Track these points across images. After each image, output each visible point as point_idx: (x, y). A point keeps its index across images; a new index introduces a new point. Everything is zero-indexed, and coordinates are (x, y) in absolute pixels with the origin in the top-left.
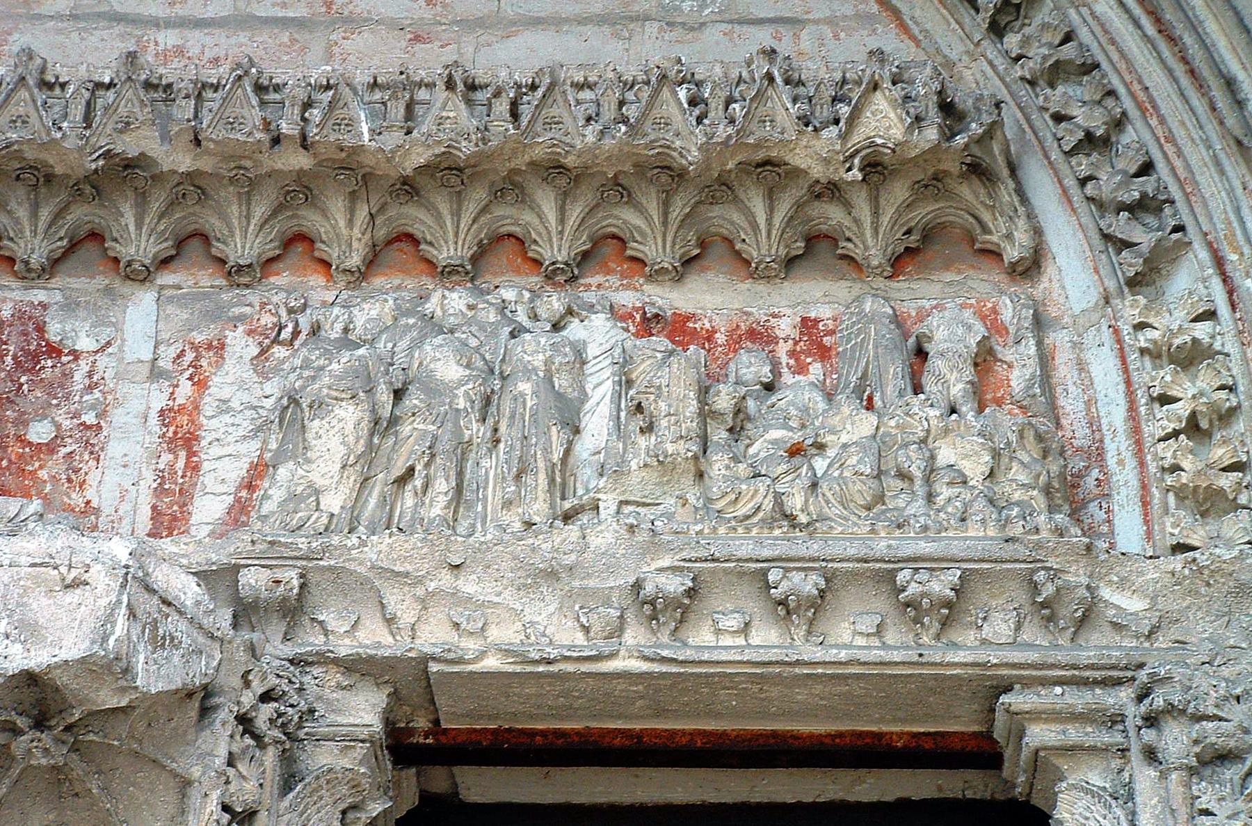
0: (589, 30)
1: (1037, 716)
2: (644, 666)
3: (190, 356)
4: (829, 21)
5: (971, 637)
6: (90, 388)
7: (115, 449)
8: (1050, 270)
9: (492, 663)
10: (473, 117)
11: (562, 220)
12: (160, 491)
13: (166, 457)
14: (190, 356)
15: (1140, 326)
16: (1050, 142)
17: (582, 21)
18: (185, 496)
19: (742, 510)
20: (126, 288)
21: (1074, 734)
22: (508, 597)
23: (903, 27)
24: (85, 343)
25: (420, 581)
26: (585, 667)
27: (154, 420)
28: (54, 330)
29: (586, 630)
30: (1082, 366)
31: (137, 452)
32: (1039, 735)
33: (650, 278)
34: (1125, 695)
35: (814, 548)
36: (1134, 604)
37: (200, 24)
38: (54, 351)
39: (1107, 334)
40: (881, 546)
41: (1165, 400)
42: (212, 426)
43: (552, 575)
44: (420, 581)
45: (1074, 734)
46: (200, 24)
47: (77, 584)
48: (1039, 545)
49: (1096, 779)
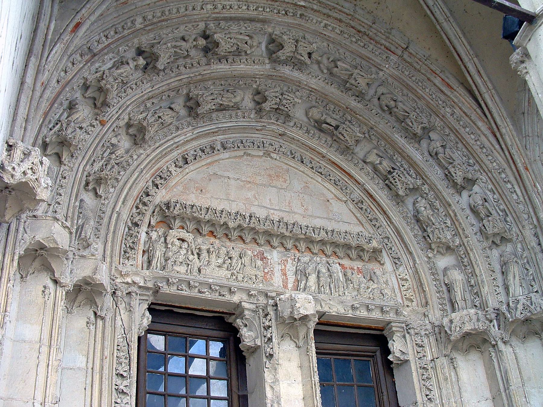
0: (325, 220)
1: (394, 326)
2: (352, 316)
3: (283, 262)
4: (354, 224)
5: (388, 316)
6: (271, 264)
7: (276, 274)
8: (385, 265)
9: (334, 314)
10: (46, 156)
11: (329, 249)
12: (283, 282)
13: (283, 277)
14: (283, 262)
15: (399, 275)
16: (386, 248)
17: (324, 218)
18: (287, 283)
19: (365, 296)
20: (273, 249)
21: (398, 329)
22: (336, 305)
23: (363, 227)
24: (269, 258)
25: (326, 301)
26: (345, 315)
27: (280, 270)
28: (265, 255)
29: (345, 310)
30: (391, 279)
31: (279, 276)
32: (394, 329)
33: (339, 258)
34: (404, 325)
35: (374, 303)
36: (406, 313)
37: (275, 210)
38: (265, 258)
39: (394, 275)
40: (382, 304)
41: (403, 286)
42: (288, 273)
43: (342, 302)
44: (326, 301)
45: (398, 329)
46: (275, 210)
47: (310, 302)
48: (398, 305)
49: (398, 335)
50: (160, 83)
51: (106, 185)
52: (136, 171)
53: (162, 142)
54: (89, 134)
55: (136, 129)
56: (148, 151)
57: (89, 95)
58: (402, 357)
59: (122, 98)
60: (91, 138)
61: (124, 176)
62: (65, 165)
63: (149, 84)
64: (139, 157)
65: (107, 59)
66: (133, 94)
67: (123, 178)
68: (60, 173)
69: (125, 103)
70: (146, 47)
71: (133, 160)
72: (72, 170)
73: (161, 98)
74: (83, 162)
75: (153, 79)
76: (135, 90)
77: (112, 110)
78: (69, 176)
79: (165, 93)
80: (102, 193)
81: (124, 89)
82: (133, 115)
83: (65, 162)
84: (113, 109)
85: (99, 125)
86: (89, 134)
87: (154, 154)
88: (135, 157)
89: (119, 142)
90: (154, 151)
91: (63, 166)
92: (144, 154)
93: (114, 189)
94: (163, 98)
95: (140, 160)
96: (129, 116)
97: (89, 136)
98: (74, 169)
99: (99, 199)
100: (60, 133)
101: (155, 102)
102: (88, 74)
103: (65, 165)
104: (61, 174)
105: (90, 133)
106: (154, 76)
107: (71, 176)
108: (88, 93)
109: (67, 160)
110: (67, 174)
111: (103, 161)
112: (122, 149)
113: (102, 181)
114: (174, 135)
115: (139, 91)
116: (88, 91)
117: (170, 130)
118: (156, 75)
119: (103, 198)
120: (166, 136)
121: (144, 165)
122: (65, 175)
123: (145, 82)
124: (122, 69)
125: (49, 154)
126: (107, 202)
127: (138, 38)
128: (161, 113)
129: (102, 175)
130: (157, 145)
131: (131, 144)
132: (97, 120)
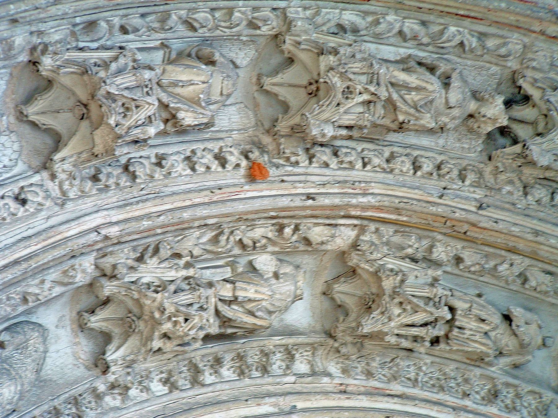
50: (518, 214)
51: (145, 345)
52: (273, 400)
53: (415, 392)
54: (193, 169)
55: (359, 293)
56: (351, 381)
57: (276, 89)
58: (67, 187)
59: (368, 167)
60: (188, 179)
61: (226, 386)
62: (53, 177)
63: (479, 194)
64: (313, 373)
65: (390, 23)
66: (408, 179)
67: (218, 387)
68: (22, 183)
69: (366, 182)
70: (536, 80)
71: (288, 367)
72: (63, 205)
73: (496, 266)
74: (112, 212)
75: (500, 190)
76: (423, 177)
77: (310, 170)
78: (39, 211)
79: (517, 259)
80: (115, 361)
81: (392, 153)
82: (373, 244)
83: (58, 167)
84: (318, 171)
85: (242, 171)
86: (193, 169)
87: (364, 402)
88: (301, 366)
89: (276, 276)
90: (371, 393)
91: (45, 174)
92: (337, 381)
93: (166, 389)
94: (500, 268)
95: (307, 384)
96: (358, 236)
97: (189, 171)
98: (70, 206)
99: (98, 371)
100: (95, 69)
101: (468, 262)
102: (301, 16)
103: (53, 177)
104: (22, 188)
105: (200, 169)
106: (511, 182)
107: (44, 214)
108: (275, 80)
109: (67, 166)
110: (39, 199)
111: (184, 273)
112: (264, 290)
113: (141, 325)
114: (467, 403)
115: (434, 185)
116: (280, 75)
117: (466, 381)
118: (518, 184)
119: (111, 378)
120: (442, 389)
121: (308, 405)
122: (30, 197)
123: (471, 177)
124: (414, 76)
125: (32, 118)
126: (117, 403)
127: (526, 40)
128: (465, 301)
129: (148, 302)
130: (397, 388)
131: (318, 327)
132: (247, 157)
